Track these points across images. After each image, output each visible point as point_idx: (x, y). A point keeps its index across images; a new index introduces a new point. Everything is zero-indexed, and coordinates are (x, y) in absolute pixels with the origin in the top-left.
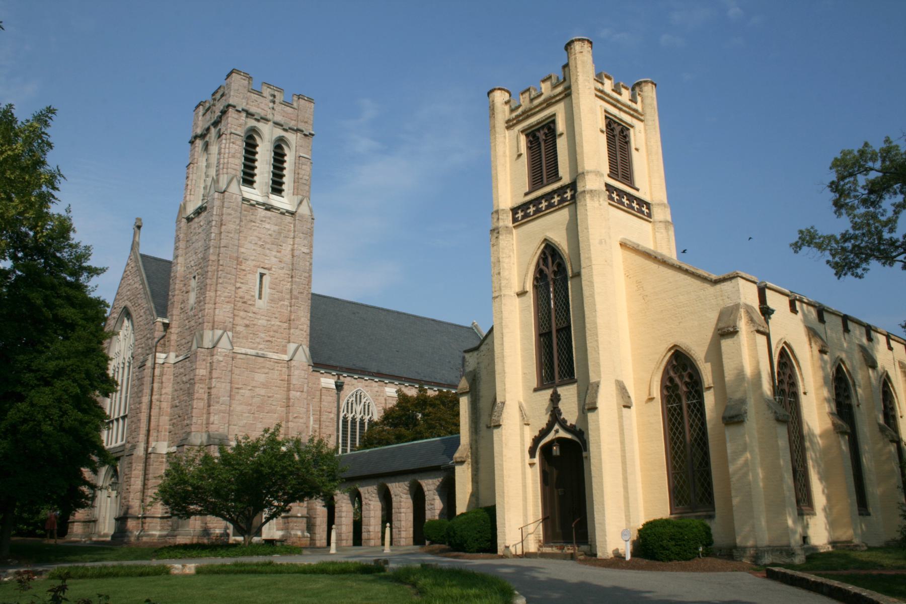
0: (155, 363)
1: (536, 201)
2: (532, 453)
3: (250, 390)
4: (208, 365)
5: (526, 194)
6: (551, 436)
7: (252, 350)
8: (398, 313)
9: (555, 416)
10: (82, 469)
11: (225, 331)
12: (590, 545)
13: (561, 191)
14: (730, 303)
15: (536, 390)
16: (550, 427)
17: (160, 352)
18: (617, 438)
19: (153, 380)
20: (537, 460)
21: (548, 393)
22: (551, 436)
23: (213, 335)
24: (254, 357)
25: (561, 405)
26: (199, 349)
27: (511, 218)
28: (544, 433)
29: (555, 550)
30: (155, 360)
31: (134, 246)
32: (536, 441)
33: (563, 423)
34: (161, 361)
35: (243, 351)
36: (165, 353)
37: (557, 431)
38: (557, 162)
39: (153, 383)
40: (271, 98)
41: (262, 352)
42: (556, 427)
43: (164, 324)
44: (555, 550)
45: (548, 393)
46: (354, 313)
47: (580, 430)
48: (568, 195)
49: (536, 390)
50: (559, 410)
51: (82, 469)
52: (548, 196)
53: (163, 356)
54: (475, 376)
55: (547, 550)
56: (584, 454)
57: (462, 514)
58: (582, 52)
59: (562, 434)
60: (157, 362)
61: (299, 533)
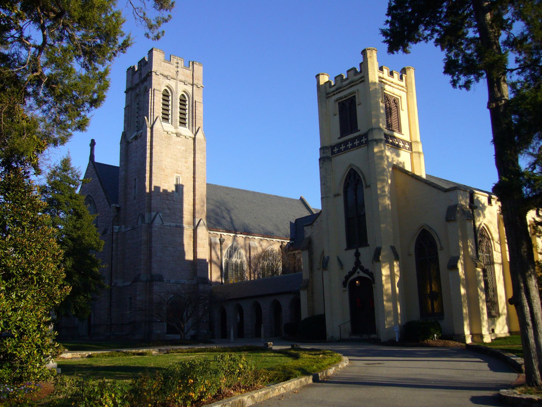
0: (113, 232)
1: (346, 143)
2: (344, 284)
3: (173, 247)
4: (149, 233)
5: (339, 138)
6: (355, 275)
7: (173, 224)
8: (254, 193)
9: (358, 264)
10: (302, 320)
11: (157, 213)
12: (377, 334)
13: (360, 138)
14: (452, 204)
15: (346, 250)
16: (354, 270)
17: (115, 225)
18: (409, 103)
19: (112, 242)
20: (347, 288)
21: (353, 251)
22: (355, 275)
23: (151, 215)
24: (174, 228)
25: (361, 259)
26: (143, 224)
27: (330, 152)
28: (351, 274)
29: (358, 337)
30: (113, 230)
31: (92, 157)
32: (347, 278)
33: (362, 268)
34: (116, 231)
35: (168, 224)
36: (119, 226)
37: (358, 273)
38: (357, 122)
39: (112, 244)
40: (176, 65)
41: (179, 224)
42: (358, 270)
43: (117, 208)
44: (358, 337)
45: (353, 251)
46: (227, 194)
47: (371, 272)
48: (364, 140)
49: (346, 250)
50: (360, 261)
51: (302, 320)
52: (353, 140)
53: (117, 227)
54: (310, 240)
55: (354, 337)
56: (373, 285)
57: (306, 319)
58: (371, 57)
59: (362, 274)
60: (114, 231)
61: (205, 331)
